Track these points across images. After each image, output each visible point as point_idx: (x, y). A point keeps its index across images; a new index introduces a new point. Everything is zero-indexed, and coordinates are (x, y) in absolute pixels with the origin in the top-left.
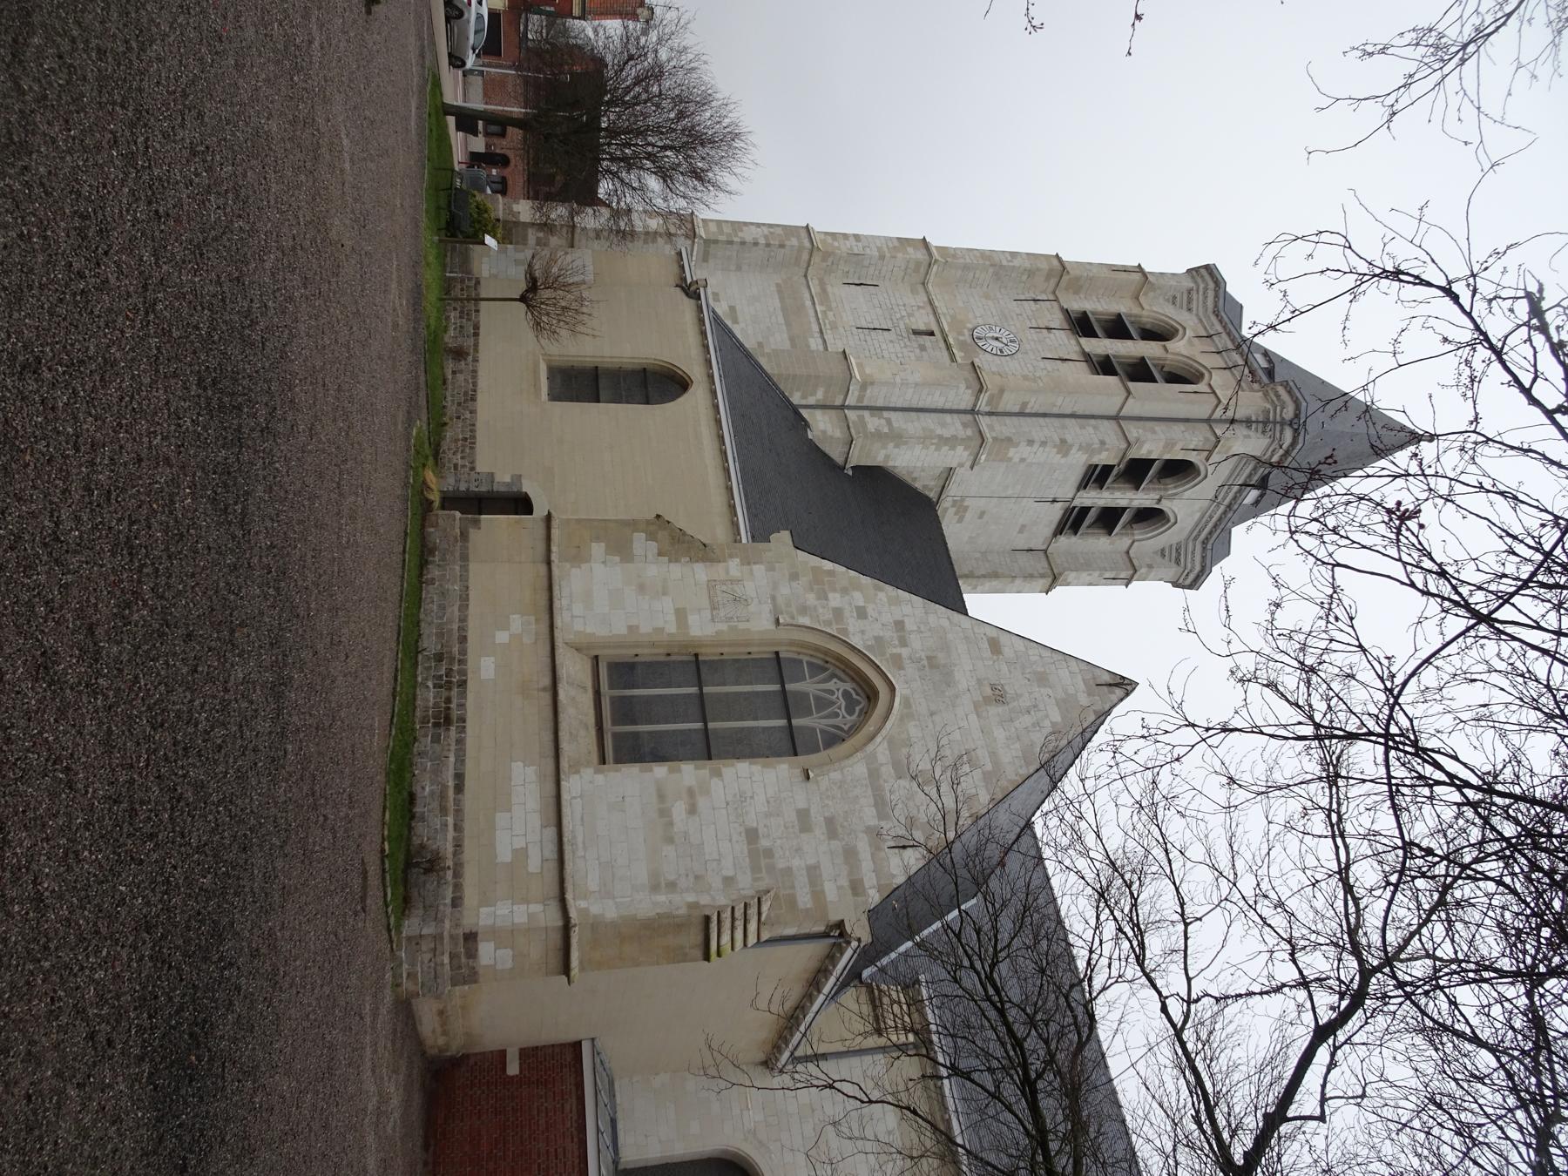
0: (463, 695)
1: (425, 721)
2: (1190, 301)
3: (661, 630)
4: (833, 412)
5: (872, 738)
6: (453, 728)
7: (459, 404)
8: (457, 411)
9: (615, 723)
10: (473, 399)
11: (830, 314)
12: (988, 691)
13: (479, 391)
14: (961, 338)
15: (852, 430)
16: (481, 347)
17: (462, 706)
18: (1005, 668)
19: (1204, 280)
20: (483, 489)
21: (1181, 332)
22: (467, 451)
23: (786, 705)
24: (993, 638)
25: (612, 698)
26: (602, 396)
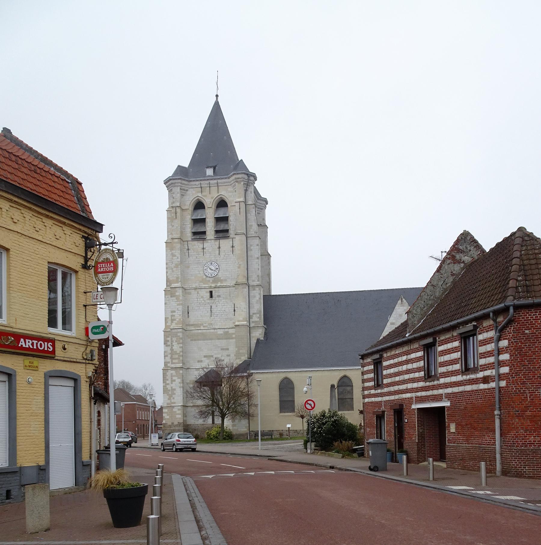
2: (184, 190)
4: (251, 331)
8: (301, 434)
10: (296, 431)
11: (204, 325)
14: (211, 281)
15: (259, 326)
19: (177, 183)
21: (200, 198)
24: (390, 324)
26: (290, 399)
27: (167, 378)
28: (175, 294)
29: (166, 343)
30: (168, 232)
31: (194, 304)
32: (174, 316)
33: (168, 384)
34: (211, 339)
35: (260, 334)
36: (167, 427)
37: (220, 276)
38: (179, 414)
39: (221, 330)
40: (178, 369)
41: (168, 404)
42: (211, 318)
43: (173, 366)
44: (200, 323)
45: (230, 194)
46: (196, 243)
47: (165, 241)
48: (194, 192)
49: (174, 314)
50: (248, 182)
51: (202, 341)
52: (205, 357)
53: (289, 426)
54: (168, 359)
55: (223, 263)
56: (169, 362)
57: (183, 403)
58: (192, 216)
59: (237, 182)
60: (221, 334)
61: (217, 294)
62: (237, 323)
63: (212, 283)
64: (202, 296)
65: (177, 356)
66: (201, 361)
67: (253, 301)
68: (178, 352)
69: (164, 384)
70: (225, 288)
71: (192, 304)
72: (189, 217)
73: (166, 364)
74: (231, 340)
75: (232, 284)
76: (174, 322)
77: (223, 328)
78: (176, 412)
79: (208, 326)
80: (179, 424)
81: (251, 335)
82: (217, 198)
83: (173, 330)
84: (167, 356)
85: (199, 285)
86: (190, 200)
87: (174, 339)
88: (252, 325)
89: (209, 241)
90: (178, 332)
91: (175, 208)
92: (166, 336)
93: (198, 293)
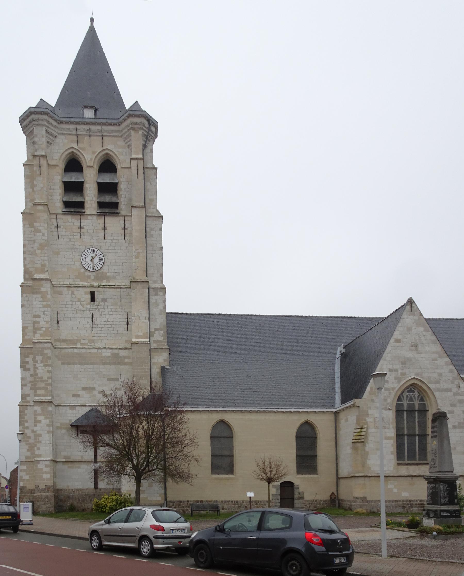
0: (413, 501)
1: (343, 513)
3: (392, 445)
5: (429, 388)
6: (424, 503)
7: (239, 507)
9: (415, 460)
10: (237, 502)
11: (83, 341)
12: (413, 348)
13: (232, 500)
14: (92, 277)
16: (211, 500)
17: (417, 501)
18: (405, 340)
19: (42, 120)
20: (279, 497)
22: (262, 503)
23: (411, 411)
25: (408, 460)
27: (26, 418)
28: (40, 289)
29: (24, 365)
30: (26, 198)
31: (66, 309)
32: (38, 323)
33: (27, 428)
34: (93, 364)
35: (165, 360)
36: (26, 493)
37: (105, 271)
38: (47, 473)
39: (108, 350)
40: (46, 404)
41: (27, 457)
42: (93, 332)
43: (37, 399)
44: (76, 338)
45: (120, 150)
46: (69, 218)
47: (22, 211)
48: (66, 141)
49: (38, 319)
50: (148, 133)
51: (78, 366)
52: (84, 389)
53: (250, 494)
54: (27, 390)
55: (110, 251)
56: (29, 395)
57: (53, 456)
58: (63, 178)
59: (133, 129)
60: (108, 357)
61: (101, 297)
62: (134, 340)
63: (94, 280)
64: (78, 299)
65: (43, 385)
66: (78, 396)
67: (155, 310)
68: (44, 379)
69: (22, 427)
70: (113, 289)
71: (64, 309)
72: (59, 177)
73: (24, 397)
74: (122, 367)
75: (123, 284)
76: (38, 332)
77: (111, 347)
78: (42, 469)
79: (89, 344)
80: (47, 488)
81: (153, 361)
82: (101, 154)
83: (36, 344)
84: (25, 385)
85: (74, 281)
86: (60, 153)
87: (39, 358)
88: (153, 346)
89: (90, 217)
90: (45, 348)
91: (38, 158)
92: (23, 356)
93: (73, 293)
